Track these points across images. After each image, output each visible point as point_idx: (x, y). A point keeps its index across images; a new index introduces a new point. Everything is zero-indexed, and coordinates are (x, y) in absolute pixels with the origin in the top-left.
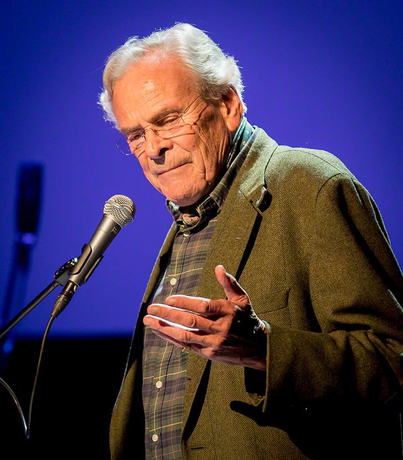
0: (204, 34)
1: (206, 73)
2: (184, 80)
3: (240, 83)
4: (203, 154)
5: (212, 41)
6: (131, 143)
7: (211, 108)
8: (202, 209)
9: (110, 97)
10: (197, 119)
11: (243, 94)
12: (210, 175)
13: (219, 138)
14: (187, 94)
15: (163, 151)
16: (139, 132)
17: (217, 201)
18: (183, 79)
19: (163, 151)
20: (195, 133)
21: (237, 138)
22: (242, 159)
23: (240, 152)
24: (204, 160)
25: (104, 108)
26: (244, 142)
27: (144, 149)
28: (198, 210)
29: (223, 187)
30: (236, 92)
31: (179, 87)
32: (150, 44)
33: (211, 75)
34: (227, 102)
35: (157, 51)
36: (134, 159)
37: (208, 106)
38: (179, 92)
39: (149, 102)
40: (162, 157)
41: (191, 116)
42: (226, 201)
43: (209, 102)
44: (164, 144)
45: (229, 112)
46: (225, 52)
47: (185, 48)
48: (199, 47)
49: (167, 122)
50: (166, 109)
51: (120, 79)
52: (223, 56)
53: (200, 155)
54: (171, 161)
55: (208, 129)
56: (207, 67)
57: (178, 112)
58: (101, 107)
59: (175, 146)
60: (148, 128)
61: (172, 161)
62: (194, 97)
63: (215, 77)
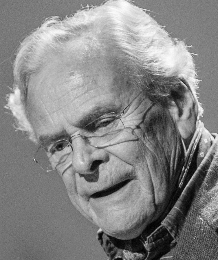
0: (145, 13)
1: (151, 61)
2: (122, 70)
3: (193, 75)
4: (150, 168)
5: (156, 23)
6: (54, 156)
7: (158, 108)
8: (151, 242)
9: (23, 97)
10: (141, 121)
11: (197, 91)
12: (160, 196)
13: (169, 147)
14: (126, 89)
15: (95, 164)
16: (61, 141)
17: (171, 231)
18: (120, 69)
19: (95, 164)
20: (138, 140)
21: (192, 148)
22: (202, 176)
23: (196, 168)
24: (152, 176)
25: (14, 113)
26: (201, 154)
27: (71, 163)
28: (146, 245)
29: (178, 213)
30: (188, 87)
31: (115, 79)
32: (74, 26)
33: (157, 64)
34: (178, 101)
35: (84, 34)
36: (57, 175)
37: (153, 105)
38: (116, 86)
39: (77, 100)
40: (94, 171)
41: (132, 117)
42: (184, 231)
43: (155, 100)
44: (97, 155)
45: (180, 113)
46: (172, 36)
47: (121, 29)
48: (140, 28)
49: (99, 127)
50: (99, 108)
51: (36, 71)
52: (169, 42)
53: (146, 169)
54: (107, 177)
55: (154, 136)
56: (152, 53)
57: (114, 113)
58: (10, 111)
59: (112, 158)
60: (76, 134)
61: (109, 178)
62: (134, 93)
63: (162, 66)
